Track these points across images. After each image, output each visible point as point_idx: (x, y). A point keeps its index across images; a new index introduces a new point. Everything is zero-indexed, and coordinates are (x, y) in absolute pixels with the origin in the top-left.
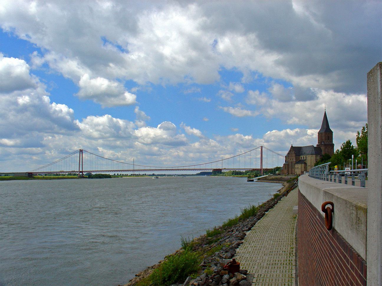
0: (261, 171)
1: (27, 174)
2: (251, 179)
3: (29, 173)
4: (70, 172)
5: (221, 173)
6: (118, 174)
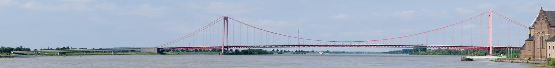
0: (489, 50)
1: (156, 49)
2: (468, 57)
3: (159, 49)
4: (213, 47)
5: (425, 50)
6: (278, 50)
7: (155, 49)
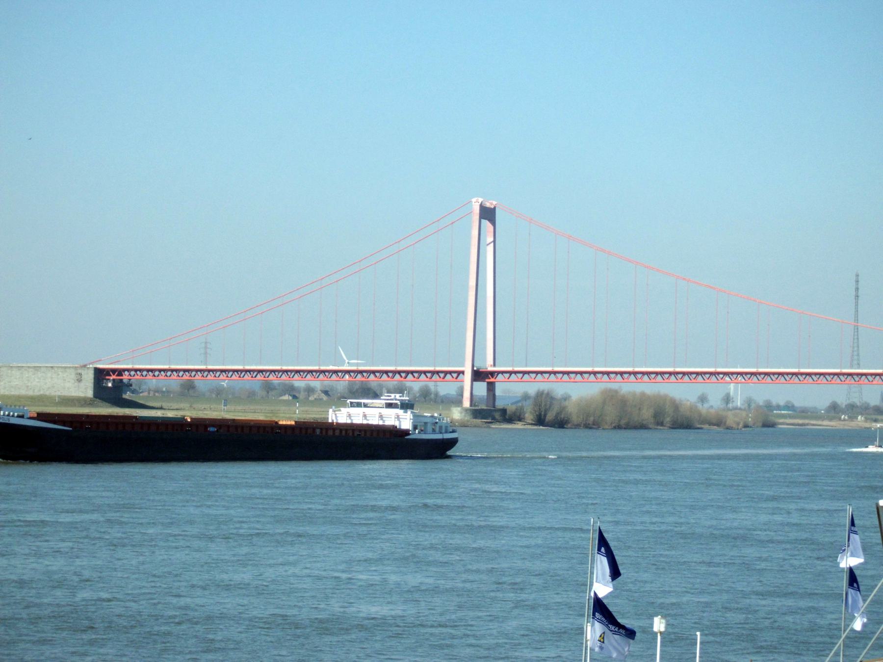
1: (89, 377)
7: (83, 372)
